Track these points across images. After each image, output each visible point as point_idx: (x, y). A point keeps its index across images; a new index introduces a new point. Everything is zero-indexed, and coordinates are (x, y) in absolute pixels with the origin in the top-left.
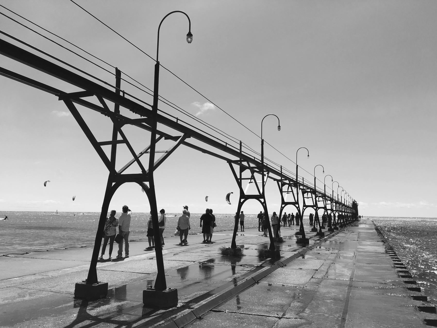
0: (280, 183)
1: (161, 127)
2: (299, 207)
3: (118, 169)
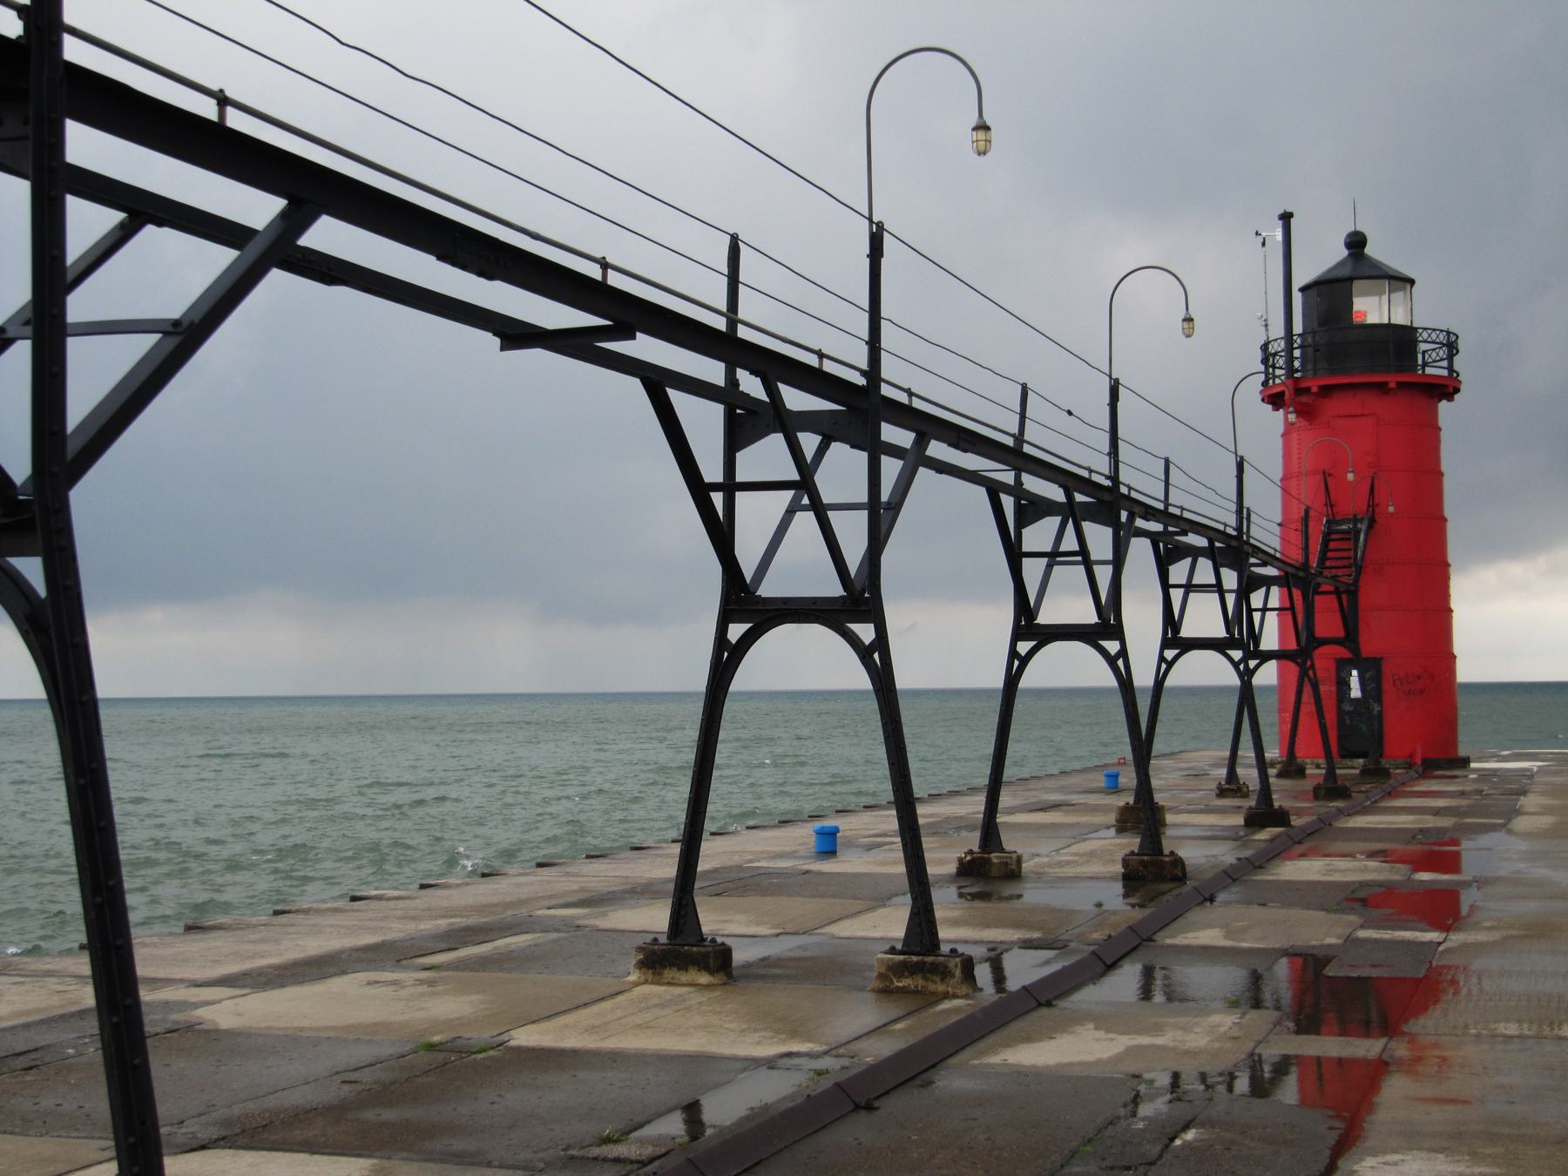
0: (1008, 502)
1: (86, 145)
2: (1123, 652)
3: (748, 554)
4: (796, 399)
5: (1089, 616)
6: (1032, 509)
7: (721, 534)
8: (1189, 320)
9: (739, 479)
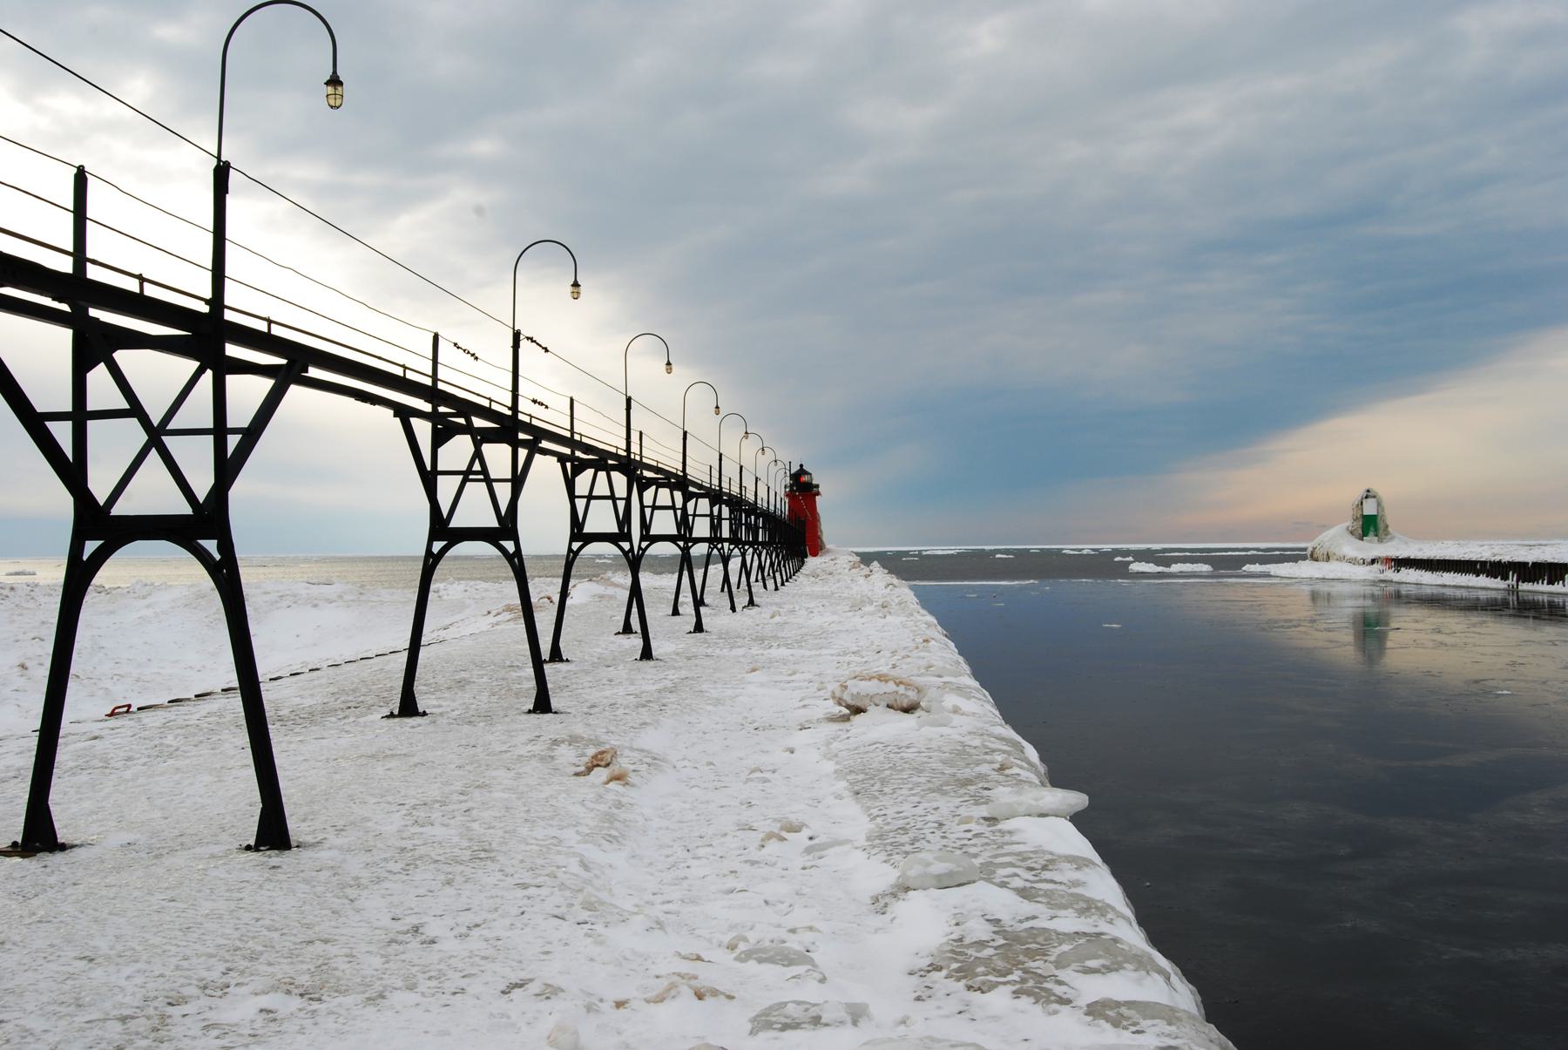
0: (568, 465)
1: (233, 350)
3: (100, 485)
4: (478, 422)
5: (613, 528)
6: (580, 466)
7: (72, 472)
8: (335, 81)
9: (91, 407)
